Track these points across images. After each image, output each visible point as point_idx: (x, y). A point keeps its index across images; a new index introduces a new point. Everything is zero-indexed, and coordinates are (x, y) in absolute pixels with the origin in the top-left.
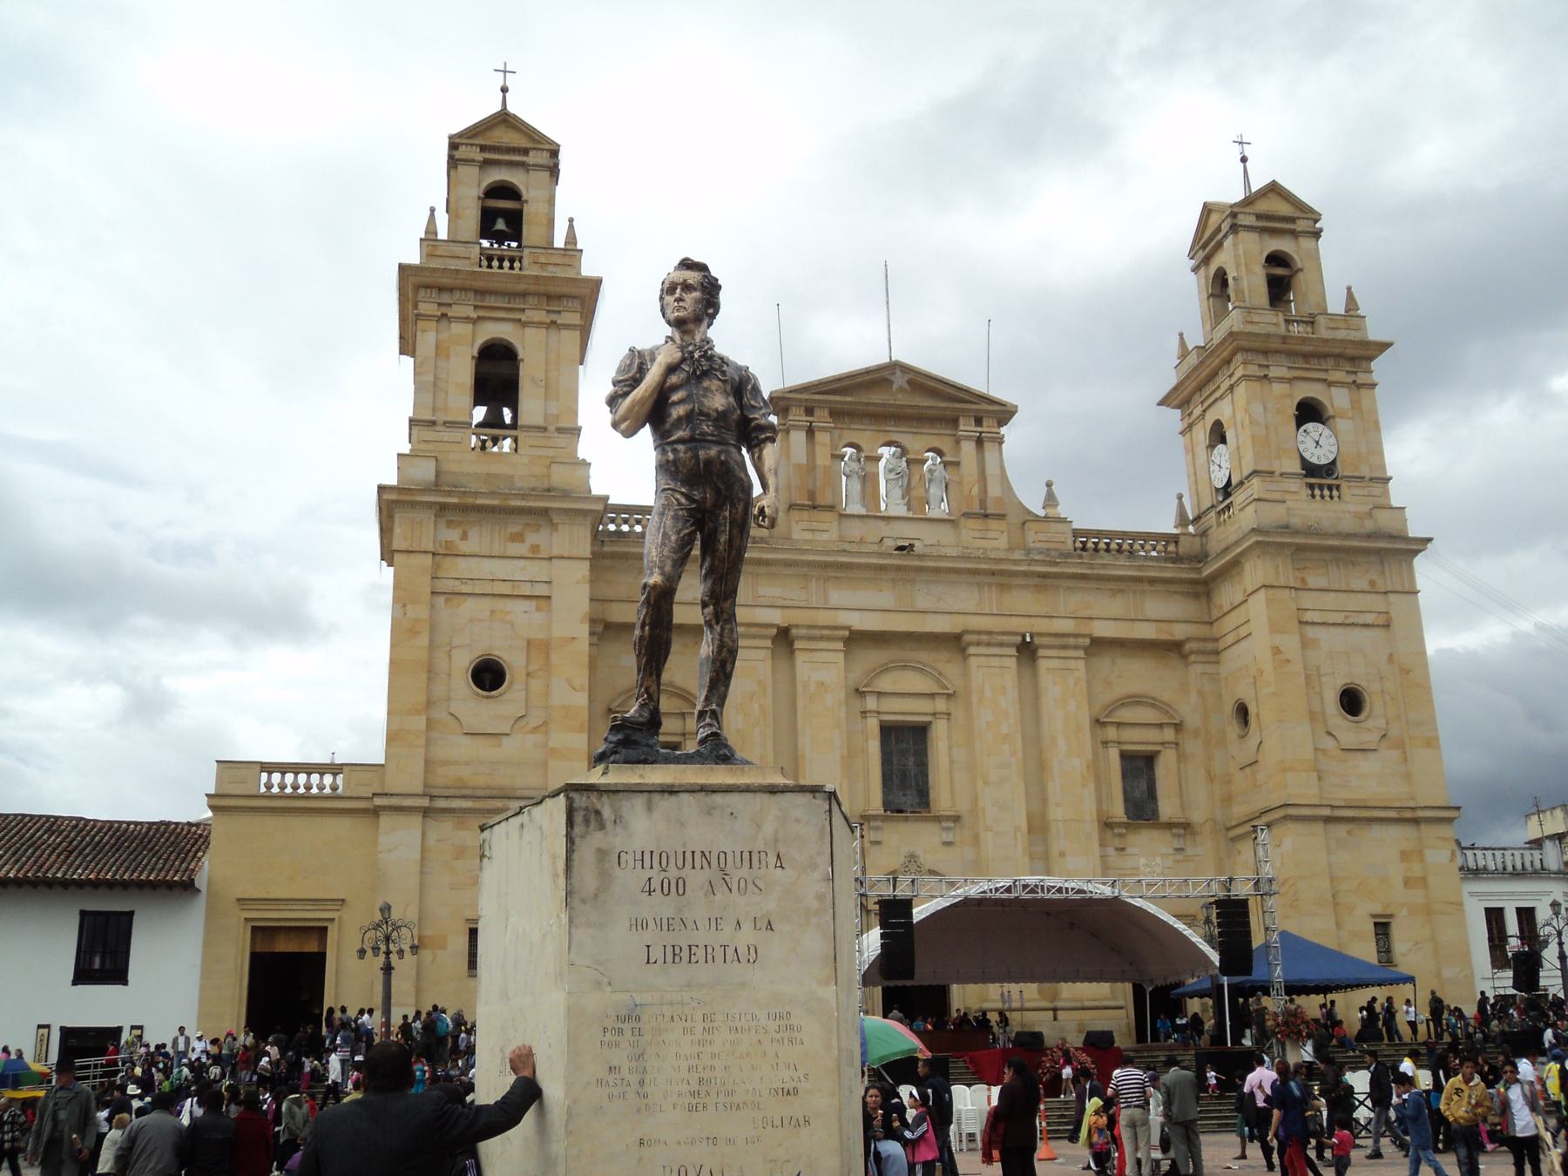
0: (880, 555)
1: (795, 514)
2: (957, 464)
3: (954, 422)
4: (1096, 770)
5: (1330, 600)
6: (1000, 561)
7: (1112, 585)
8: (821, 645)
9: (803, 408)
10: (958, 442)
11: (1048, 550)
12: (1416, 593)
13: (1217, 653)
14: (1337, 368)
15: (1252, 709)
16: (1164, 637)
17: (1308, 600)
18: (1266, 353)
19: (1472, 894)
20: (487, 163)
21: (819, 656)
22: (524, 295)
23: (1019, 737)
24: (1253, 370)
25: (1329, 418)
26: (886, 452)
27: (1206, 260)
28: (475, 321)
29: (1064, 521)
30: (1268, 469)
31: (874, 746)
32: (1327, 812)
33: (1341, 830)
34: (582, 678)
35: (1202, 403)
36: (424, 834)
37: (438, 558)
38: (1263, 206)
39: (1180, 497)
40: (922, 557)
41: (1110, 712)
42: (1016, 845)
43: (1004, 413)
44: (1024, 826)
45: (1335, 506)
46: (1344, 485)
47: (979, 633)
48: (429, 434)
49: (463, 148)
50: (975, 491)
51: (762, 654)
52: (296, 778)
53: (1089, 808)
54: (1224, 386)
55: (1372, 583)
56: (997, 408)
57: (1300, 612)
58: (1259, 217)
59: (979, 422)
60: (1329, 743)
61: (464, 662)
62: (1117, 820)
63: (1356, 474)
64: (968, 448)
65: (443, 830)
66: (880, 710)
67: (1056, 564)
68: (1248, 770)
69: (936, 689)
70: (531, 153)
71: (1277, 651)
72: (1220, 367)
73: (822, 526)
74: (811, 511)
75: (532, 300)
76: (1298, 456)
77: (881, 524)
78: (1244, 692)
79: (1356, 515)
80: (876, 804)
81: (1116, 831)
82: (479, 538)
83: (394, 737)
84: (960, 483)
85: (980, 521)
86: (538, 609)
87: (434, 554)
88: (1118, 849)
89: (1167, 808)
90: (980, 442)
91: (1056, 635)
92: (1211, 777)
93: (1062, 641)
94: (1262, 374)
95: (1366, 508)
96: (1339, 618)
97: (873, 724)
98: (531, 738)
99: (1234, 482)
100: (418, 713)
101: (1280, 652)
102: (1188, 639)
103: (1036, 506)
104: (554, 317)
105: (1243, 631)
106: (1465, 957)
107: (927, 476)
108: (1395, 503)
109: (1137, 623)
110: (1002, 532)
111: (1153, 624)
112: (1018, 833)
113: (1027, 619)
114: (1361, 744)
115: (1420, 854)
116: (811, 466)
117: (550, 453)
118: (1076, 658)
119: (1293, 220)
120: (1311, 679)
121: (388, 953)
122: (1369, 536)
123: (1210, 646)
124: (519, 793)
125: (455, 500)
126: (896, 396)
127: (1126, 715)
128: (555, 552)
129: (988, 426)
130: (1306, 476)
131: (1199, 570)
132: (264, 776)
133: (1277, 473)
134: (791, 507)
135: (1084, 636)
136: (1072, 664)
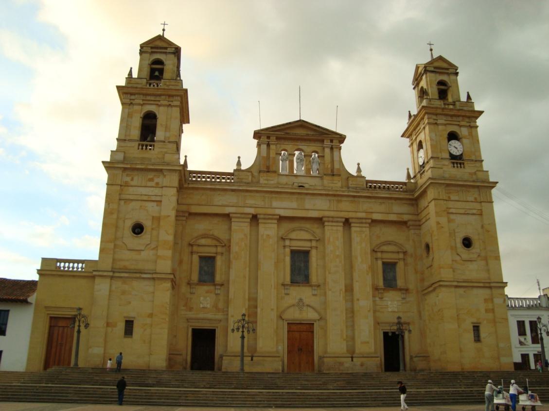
0: (292, 188)
1: (262, 174)
2: (323, 157)
3: (323, 141)
4: (372, 268)
5: (459, 205)
6: (337, 191)
7: (380, 201)
8: (270, 221)
9: (266, 137)
10: (324, 148)
11: (357, 187)
12: (493, 202)
13: (420, 226)
14: (463, 121)
15: (430, 245)
16: (401, 220)
17: (450, 204)
18: (436, 115)
19: (512, 315)
20: (152, 53)
21: (267, 225)
22: (160, 95)
23: (343, 256)
24: (432, 121)
25: (460, 138)
26: (297, 153)
27: (418, 85)
28: (142, 105)
29: (364, 177)
30: (437, 156)
31: (288, 259)
32: (455, 284)
33: (461, 291)
34: (171, 231)
35: (415, 135)
36: (111, 286)
37: (122, 187)
38: (436, 64)
39: (408, 169)
40: (307, 189)
41: (379, 247)
42: (340, 296)
43: (342, 138)
44: (344, 290)
45: (462, 170)
46: (466, 163)
47: (328, 217)
48: (123, 144)
49: (144, 48)
50: (329, 166)
51: (246, 224)
52: (65, 265)
53: (369, 281)
54: (422, 127)
55: (476, 199)
56: (338, 136)
57: (448, 209)
58: (435, 68)
59: (332, 141)
60: (458, 258)
61: (129, 224)
62: (381, 287)
63: (470, 159)
64: (327, 151)
65: (118, 284)
66: (291, 245)
67: (359, 192)
68: (429, 269)
69: (312, 238)
70: (169, 49)
71: (438, 223)
72: (420, 121)
73: (271, 179)
74: (268, 173)
75: (163, 97)
76: (448, 152)
77: (294, 178)
78: (428, 239)
79: (470, 174)
80: (288, 279)
81: (380, 291)
82: (138, 179)
83: (102, 250)
84: (324, 164)
85: (330, 177)
86: (157, 205)
87: (121, 186)
88: (380, 298)
89: (400, 283)
90: (332, 148)
91: (358, 218)
92: (416, 272)
93: (360, 220)
94: (434, 122)
95: (473, 171)
96: (462, 211)
97: (288, 250)
98: (152, 252)
99: (425, 162)
100: (111, 242)
101: (439, 224)
102: (409, 220)
103: (353, 171)
104: (170, 103)
105: (428, 217)
106: (508, 339)
107: (312, 161)
108: (485, 169)
109: (389, 215)
110: (339, 181)
111: (396, 215)
112: (341, 292)
113: (347, 213)
114: (470, 258)
115: (492, 300)
116: (268, 157)
117: (165, 150)
118: (365, 227)
119: (448, 69)
120: (452, 234)
121: (243, 332)
122: (474, 181)
123: (417, 223)
124: (146, 272)
125: (129, 166)
126: (301, 132)
127: (385, 248)
128: (164, 185)
129: (335, 143)
130: (451, 159)
131: (413, 195)
132: (58, 264)
133: (440, 158)
134: (260, 172)
135: (369, 219)
136: (364, 229)
